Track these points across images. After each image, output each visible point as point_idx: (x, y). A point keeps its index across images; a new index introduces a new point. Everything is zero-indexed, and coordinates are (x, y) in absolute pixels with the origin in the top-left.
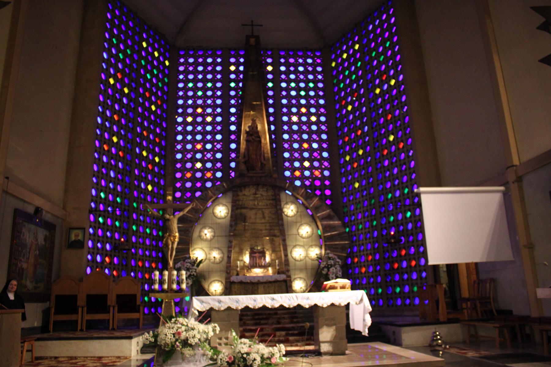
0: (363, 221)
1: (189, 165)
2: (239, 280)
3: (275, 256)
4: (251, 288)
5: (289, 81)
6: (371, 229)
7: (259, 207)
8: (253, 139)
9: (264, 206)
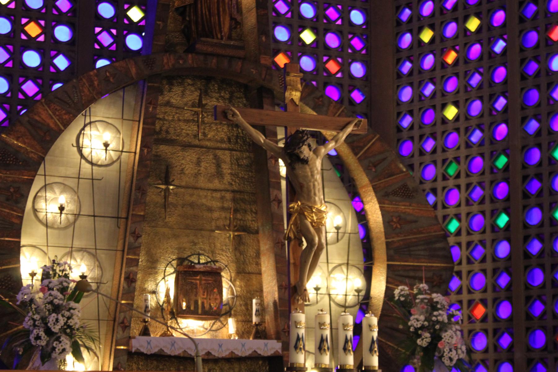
0: (464, 210)
2: (155, 350)
3: (243, 284)
6: (488, 237)
7: (208, 144)
9: (222, 141)
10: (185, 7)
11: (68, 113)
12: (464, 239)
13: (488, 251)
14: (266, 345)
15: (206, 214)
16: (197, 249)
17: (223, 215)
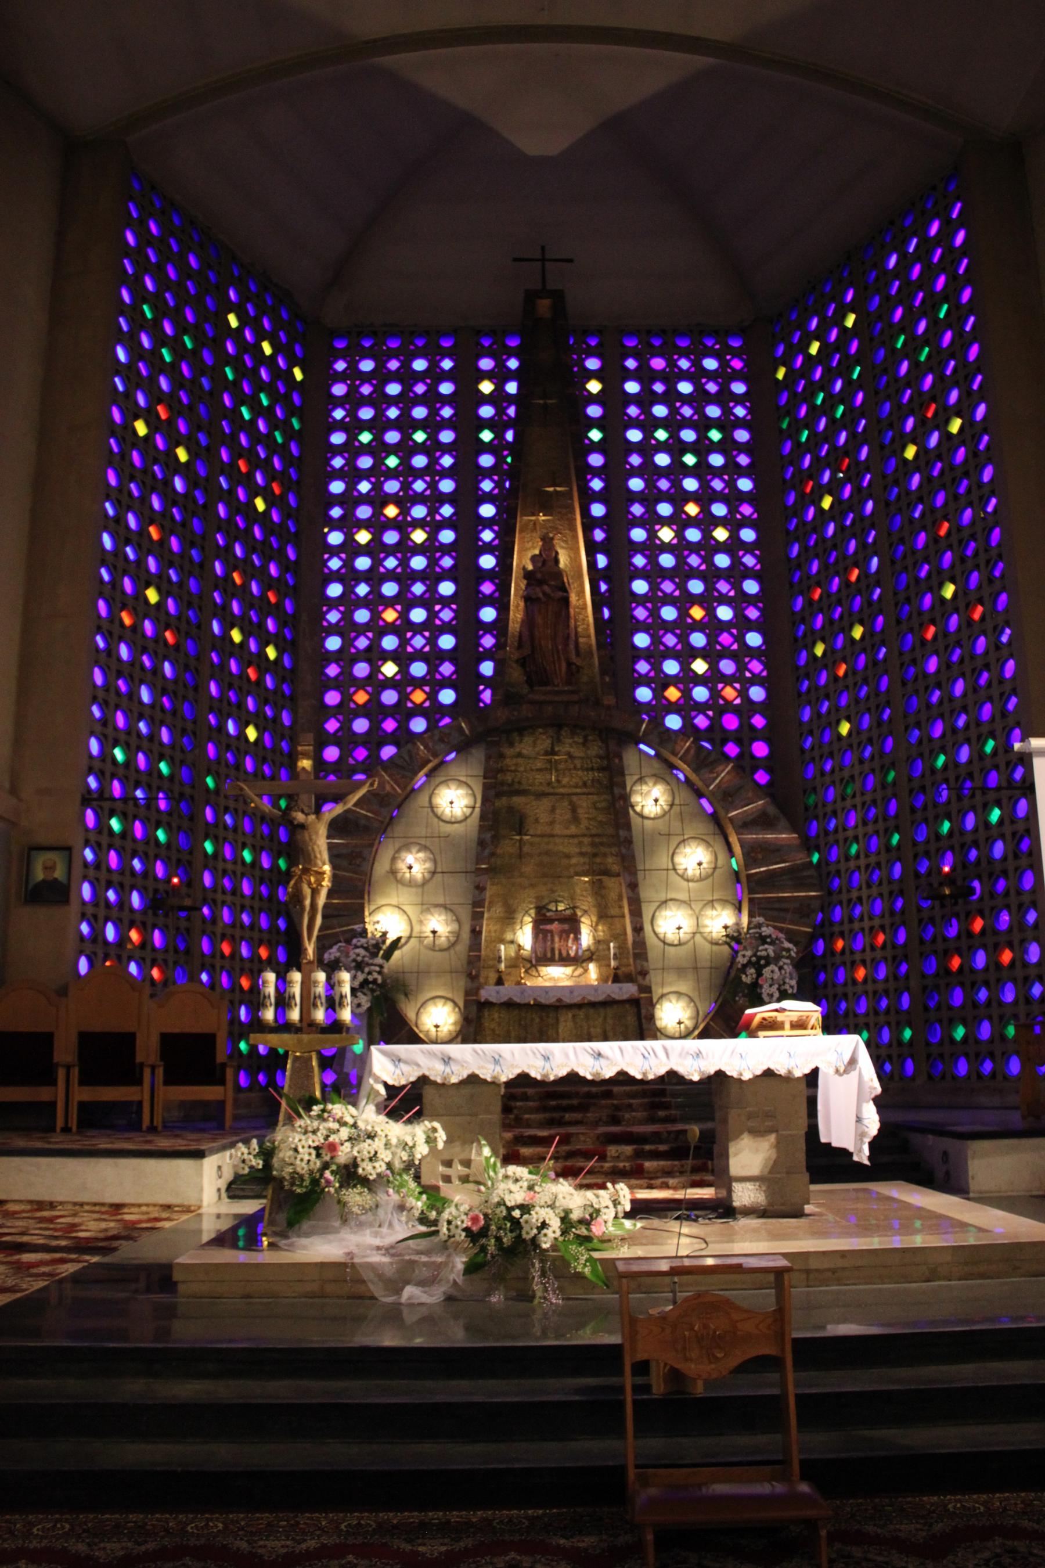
1: (361, 669)
2: (504, 999)
3: (605, 928)
4: (537, 1020)
5: (649, 424)
6: (883, 858)
7: (562, 790)
8: (545, 594)
10: (524, 658)
11: (403, 777)
12: (862, 862)
13: (884, 873)
14: (621, 989)
15: (565, 861)
16: (555, 896)
17: (582, 860)
